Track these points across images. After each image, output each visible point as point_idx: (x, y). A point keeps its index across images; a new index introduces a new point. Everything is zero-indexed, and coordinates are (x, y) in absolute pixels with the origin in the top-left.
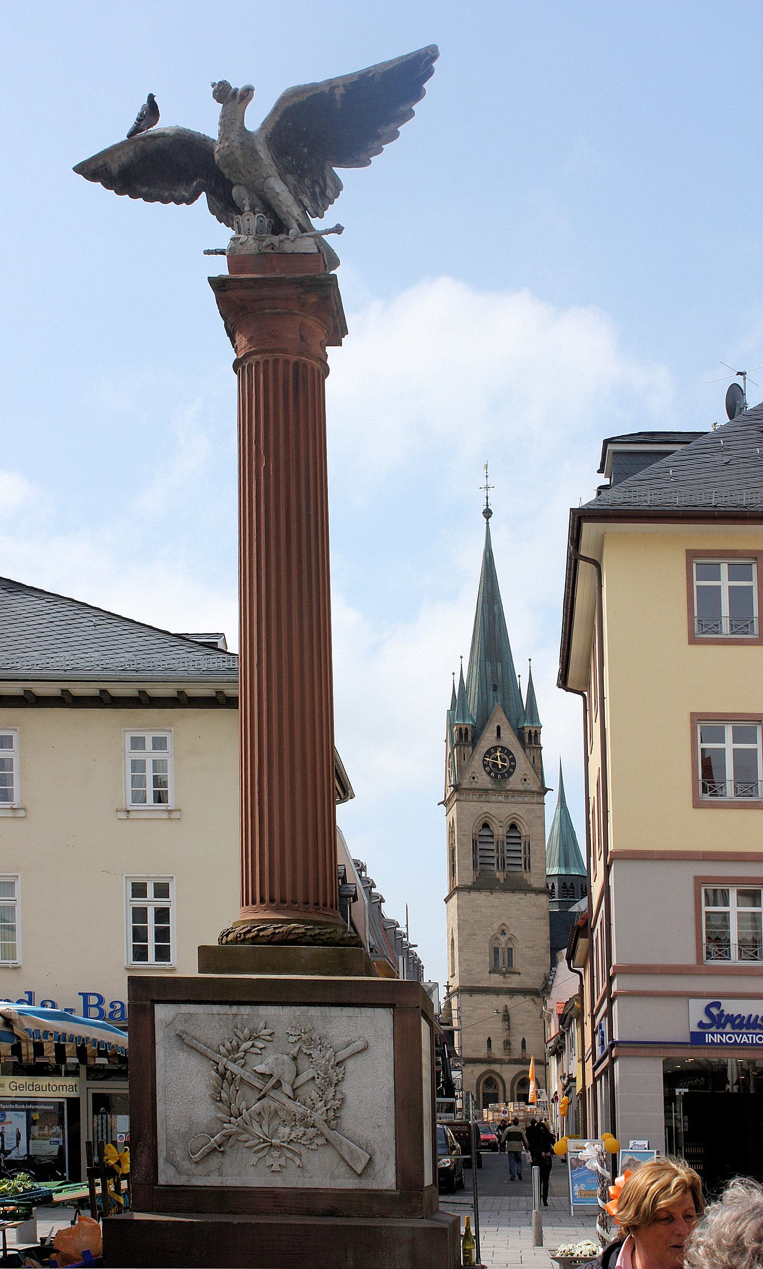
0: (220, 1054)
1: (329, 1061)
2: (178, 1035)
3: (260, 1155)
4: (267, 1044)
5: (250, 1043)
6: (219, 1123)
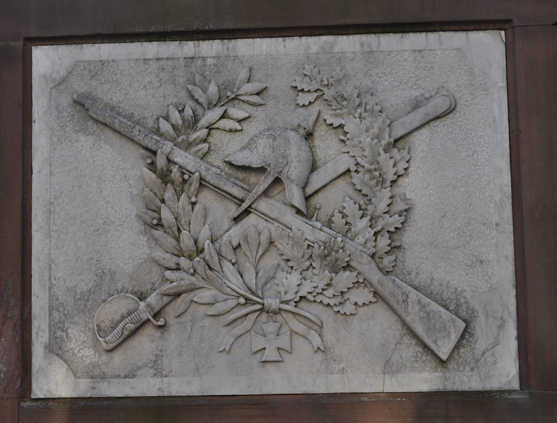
0: (161, 135)
1: (378, 137)
2: (75, 102)
3: (239, 329)
4: (252, 110)
5: (219, 111)
6: (156, 270)
